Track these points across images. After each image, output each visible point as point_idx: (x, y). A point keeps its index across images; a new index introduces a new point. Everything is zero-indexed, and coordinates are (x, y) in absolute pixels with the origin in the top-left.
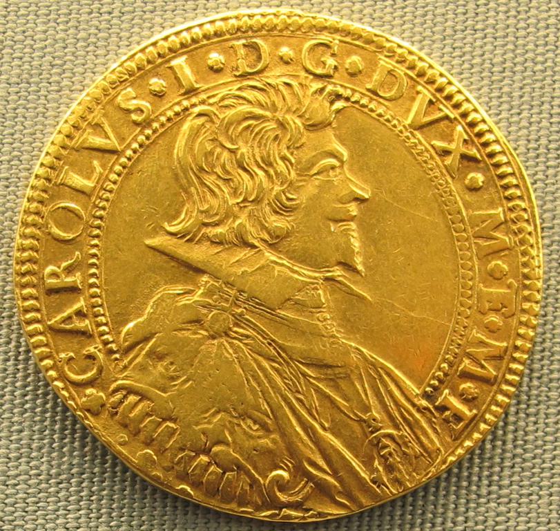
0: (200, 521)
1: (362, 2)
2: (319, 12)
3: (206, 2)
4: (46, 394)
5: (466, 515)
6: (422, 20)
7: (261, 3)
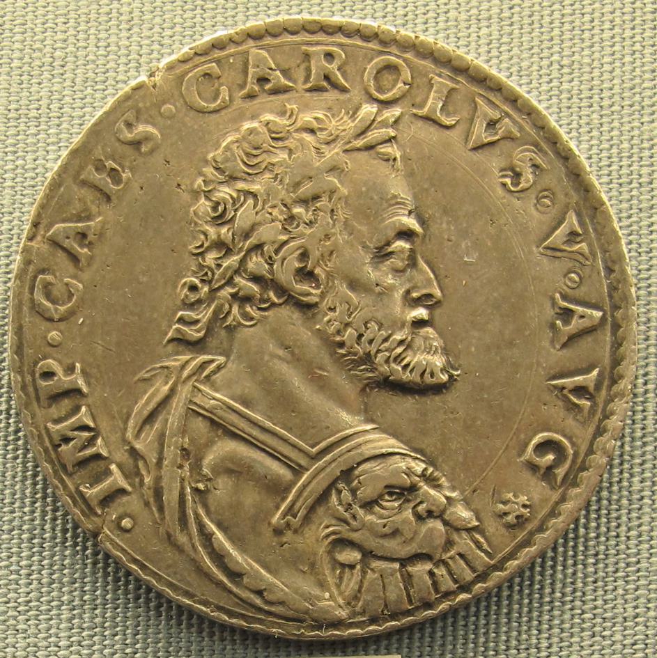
1: (173, 3)
2: (299, 13)
3: (203, 3)
4: (159, 606)
5: (561, 618)
6: (424, 27)
7: (48, 4)
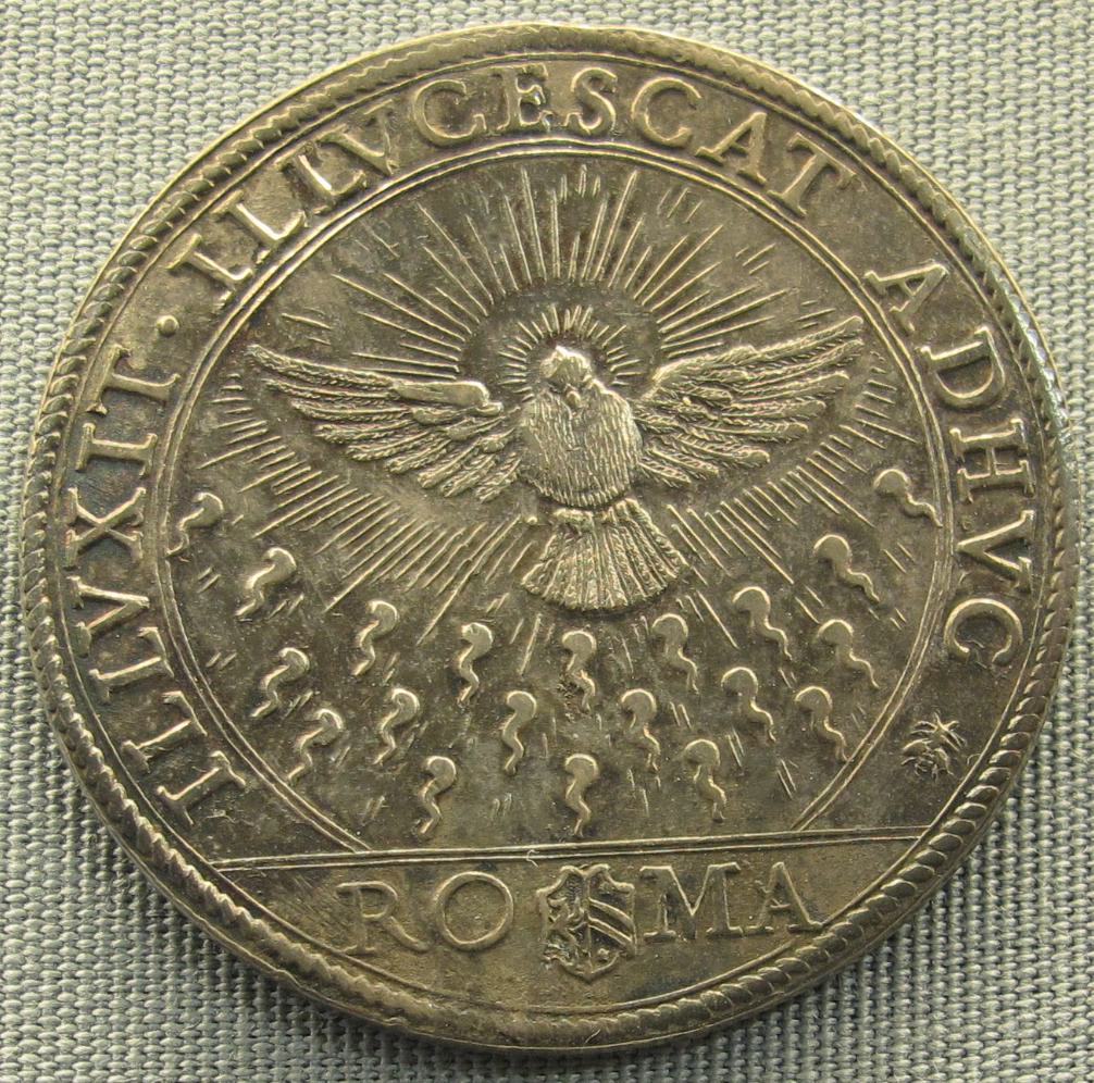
0: (421, 1070)
